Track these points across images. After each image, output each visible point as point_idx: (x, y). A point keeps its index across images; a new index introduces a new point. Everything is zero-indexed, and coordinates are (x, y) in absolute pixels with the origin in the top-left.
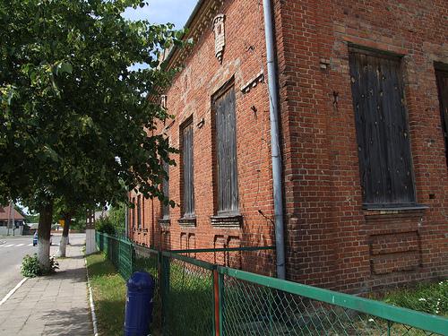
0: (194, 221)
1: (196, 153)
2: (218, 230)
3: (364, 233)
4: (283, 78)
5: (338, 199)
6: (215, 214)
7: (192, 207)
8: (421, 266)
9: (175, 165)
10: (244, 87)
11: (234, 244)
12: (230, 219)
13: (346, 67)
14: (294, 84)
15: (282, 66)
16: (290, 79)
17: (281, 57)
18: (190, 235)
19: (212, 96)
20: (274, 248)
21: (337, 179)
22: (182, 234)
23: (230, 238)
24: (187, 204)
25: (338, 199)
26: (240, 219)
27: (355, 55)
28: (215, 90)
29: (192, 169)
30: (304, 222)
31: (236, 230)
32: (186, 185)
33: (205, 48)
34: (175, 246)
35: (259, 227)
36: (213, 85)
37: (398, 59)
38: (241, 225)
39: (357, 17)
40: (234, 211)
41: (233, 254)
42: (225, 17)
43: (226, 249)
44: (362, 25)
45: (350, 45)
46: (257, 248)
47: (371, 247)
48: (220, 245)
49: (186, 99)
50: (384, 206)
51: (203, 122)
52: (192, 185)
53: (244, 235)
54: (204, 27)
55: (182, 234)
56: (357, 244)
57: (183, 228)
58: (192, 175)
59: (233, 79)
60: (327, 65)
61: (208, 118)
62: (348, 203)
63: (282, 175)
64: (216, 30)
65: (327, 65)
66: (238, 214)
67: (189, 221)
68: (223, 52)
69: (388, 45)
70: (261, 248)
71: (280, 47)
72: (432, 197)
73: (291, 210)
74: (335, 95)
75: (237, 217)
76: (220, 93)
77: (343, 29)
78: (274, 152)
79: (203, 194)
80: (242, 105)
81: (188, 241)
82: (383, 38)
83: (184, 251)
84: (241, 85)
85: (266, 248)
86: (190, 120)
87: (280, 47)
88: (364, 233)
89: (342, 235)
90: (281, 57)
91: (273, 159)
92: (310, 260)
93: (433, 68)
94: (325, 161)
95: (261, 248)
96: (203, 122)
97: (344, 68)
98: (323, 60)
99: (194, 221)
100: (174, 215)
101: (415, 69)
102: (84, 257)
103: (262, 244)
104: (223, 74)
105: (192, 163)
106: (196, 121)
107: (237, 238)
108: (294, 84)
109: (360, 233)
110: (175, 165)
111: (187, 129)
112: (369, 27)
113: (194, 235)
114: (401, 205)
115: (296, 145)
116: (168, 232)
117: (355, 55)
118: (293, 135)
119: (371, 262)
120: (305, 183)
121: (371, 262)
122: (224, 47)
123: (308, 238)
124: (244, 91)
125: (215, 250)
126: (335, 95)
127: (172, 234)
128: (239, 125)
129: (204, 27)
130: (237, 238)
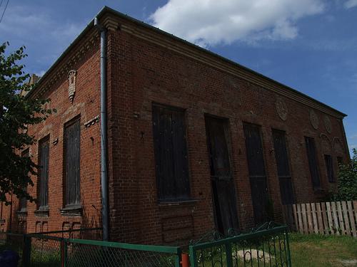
0: (47, 213)
1: (51, 162)
2: (65, 218)
3: (158, 217)
4: (110, 124)
5: (142, 197)
6: (64, 207)
7: (47, 202)
8: (194, 236)
9: (33, 185)
10: (86, 123)
11: (77, 227)
12: (74, 211)
13: (150, 116)
14: (117, 127)
15: (110, 115)
16: (114, 124)
17: (110, 110)
18: (44, 223)
19: (65, 124)
20: (102, 228)
21: (141, 185)
22: (37, 222)
23: (74, 224)
24: (41, 200)
25: (142, 197)
26: (80, 211)
27: (156, 109)
28: (67, 120)
29: (48, 173)
30: (120, 211)
31: (78, 218)
32: (42, 186)
33: (61, 89)
34: (30, 231)
35: (93, 215)
36: (66, 118)
37: (183, 111)
38: (82, 215)
39: (159, 85)
40: (77, 205)
41: (76, 234)
42: (76, 73)
43: (70, 231)
44: (162, 90)
45: (153, 102)
46: (92, 229)
47: (163, 226)
48: (66, 228)
49: (46, 128)
50: (171, 201)
51: (57, 141)
52: (47, 186)
53: (84, 222)
54: (62, 75)
55: (37, 222)
56: (153, 224)
57: (37, 218)
58: (47, 178)
59: (79, 115)
60: (138, 115)
61: (61, 139)
62: (148, 200)
63: (107, 182)
64: (70, 79)
65: (138, 115)
66: (80, 207)
67: (44, 212)
68: (74, 96)
69: (176, 103)
70: (94, 229)
71: (110, 104)
72: (201, 194)
73: (112, 205)
74: (143, 133)
75: (80, 209)
76: (70, 123)
77: (150, 93)
78: (103, 168)
79: (56, 193)
80: (85, 135)
81: (42, 228)
82: (174, 99)
83: (45, 233)
84: (85, 121)
85: (97, 228)
86: (47, 138)
87: (110, 104)
88: (158, 217)
89: (144, 219)
90: (110, 110)
91: (102, 173)
92: (123, 235)
93: (203, 118)
94: (134, 175)
95: (94, 229)
96: (57, 141)
97: (149, 117)
98: (136, 113)
99: (47, 213)
100: (31, 207)
101: (193, 117)
102: (258, 256)
103: (94, 227)
104: (72, 110)
105: (48, 169)
106: (52, 139)
107: (79, 223)
108: (117, 127)
109: (156, 218)
110: (33, 185)
111: (45, 144)
112: (165, 92)
113: (47, 222)
114: (182, 200)
115: (116, 165)
116: (25, 222)
117: (156, 109)
118: (115, 159)
119: (163, 235)
120: (121, 188)
121: (163, 235)
122: (75, 93)
123: (123, 222)
124: (86, 126)
125: (63, 231)
126: (143, 133)
127: (29, 223)
128: (83, 147)
129: (62, 75)
130: (79, 223)
